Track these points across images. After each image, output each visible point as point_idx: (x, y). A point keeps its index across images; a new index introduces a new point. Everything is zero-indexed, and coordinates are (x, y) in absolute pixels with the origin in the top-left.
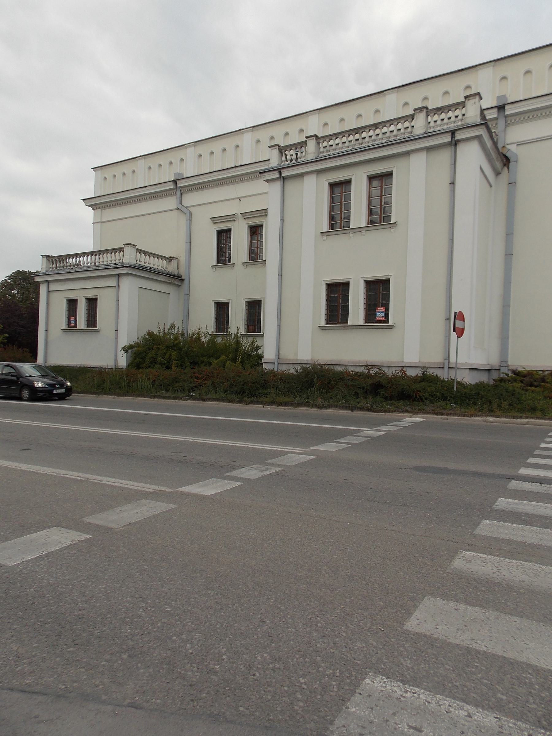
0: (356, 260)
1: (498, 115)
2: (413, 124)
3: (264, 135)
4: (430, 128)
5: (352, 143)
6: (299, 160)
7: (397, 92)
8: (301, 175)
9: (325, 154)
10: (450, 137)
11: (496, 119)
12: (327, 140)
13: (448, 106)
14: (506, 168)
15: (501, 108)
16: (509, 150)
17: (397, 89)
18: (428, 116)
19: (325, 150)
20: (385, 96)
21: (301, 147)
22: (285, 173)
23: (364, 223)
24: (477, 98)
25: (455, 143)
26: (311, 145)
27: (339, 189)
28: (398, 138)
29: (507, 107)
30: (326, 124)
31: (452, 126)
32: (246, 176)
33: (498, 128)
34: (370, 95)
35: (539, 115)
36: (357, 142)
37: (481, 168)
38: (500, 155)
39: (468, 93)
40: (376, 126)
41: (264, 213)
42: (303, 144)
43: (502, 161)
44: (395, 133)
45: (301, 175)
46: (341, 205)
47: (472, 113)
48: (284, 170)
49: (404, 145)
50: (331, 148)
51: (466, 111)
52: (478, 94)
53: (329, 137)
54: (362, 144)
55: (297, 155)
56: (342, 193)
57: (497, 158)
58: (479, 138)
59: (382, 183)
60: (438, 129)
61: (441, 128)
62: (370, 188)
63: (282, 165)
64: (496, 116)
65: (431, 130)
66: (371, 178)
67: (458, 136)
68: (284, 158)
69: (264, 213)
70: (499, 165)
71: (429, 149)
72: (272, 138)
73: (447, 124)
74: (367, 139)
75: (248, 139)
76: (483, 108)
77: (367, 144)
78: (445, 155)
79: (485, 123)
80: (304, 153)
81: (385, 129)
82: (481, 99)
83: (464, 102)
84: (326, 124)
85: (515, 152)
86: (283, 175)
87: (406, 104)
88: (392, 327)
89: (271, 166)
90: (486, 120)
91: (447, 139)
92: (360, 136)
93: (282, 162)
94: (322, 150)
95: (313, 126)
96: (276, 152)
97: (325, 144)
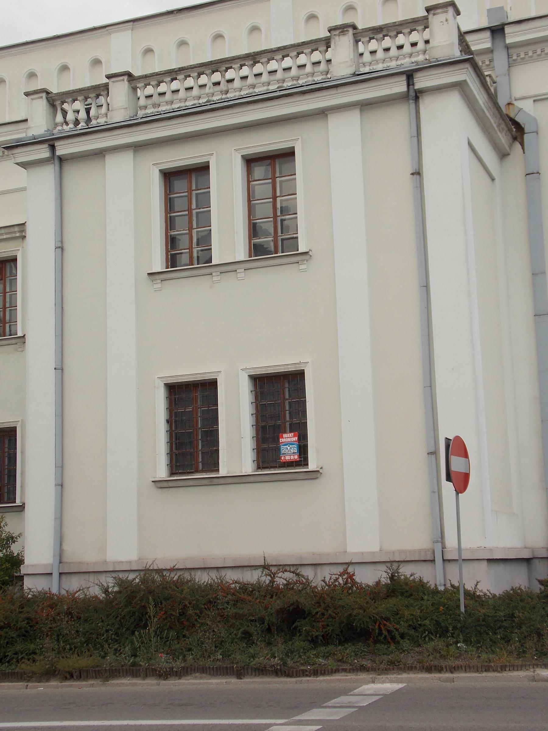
0: (230, 333)
1: (493, 43)
2: (328, 56)
5: (207, 90)
6: (94, 122)
8: (100, 154)
9: (149, 111)
10: (405, 83)
11: (490, 51)
14: (517, 145)
15: (497, 31)
16: (520, 110)
18: (357, 42)
19: (150, 101)
21: (98, 96)
22: (62, 149)
24: (451, 10)
25: (415, 96)
26: (119, 92)
27: (185, 182)
28: (301, 82)
29: (507, 30)
30: (149, 51)
31: (407, 63)
33: (496, 67)
36: (217, 88)
37: (470, 144)
38: (503, 120)
40: (253, 58)
42: (101, 90)
43: (510, 130)
45: (100, 154)
46: (190, 215)
47: (442, 39)
49: (316, 96)
50: (162, 99)
51: (431, 34)
53: (158, 77)
54: (227, 92)
55: (88, 111)
56: (190, 191)
57: (499, 126)
58: (460, 86)
60: (380, 67)
63: (55, 131)
64: (488, 45)
65: (367, 70)
66: (250, 161)
67: (421, 82)
68: (59, 118)
69: (19, 231)
70: (503, 138)
71: (365, 106)
73: (411, 55)
76: (464, 29)
78: (398, 118)
79: (469, 59)
81: (273, 65)
82: (458, 13)
83: (426, 18)
85: (531, 113)
86: (59, 152)
87: (312, 17)
88: (315, 474)
90: (471, 53)
91: (399, 86)
92: (223, 76)
93: (56, 125)
95: (122, 55)
97: (149, 90)
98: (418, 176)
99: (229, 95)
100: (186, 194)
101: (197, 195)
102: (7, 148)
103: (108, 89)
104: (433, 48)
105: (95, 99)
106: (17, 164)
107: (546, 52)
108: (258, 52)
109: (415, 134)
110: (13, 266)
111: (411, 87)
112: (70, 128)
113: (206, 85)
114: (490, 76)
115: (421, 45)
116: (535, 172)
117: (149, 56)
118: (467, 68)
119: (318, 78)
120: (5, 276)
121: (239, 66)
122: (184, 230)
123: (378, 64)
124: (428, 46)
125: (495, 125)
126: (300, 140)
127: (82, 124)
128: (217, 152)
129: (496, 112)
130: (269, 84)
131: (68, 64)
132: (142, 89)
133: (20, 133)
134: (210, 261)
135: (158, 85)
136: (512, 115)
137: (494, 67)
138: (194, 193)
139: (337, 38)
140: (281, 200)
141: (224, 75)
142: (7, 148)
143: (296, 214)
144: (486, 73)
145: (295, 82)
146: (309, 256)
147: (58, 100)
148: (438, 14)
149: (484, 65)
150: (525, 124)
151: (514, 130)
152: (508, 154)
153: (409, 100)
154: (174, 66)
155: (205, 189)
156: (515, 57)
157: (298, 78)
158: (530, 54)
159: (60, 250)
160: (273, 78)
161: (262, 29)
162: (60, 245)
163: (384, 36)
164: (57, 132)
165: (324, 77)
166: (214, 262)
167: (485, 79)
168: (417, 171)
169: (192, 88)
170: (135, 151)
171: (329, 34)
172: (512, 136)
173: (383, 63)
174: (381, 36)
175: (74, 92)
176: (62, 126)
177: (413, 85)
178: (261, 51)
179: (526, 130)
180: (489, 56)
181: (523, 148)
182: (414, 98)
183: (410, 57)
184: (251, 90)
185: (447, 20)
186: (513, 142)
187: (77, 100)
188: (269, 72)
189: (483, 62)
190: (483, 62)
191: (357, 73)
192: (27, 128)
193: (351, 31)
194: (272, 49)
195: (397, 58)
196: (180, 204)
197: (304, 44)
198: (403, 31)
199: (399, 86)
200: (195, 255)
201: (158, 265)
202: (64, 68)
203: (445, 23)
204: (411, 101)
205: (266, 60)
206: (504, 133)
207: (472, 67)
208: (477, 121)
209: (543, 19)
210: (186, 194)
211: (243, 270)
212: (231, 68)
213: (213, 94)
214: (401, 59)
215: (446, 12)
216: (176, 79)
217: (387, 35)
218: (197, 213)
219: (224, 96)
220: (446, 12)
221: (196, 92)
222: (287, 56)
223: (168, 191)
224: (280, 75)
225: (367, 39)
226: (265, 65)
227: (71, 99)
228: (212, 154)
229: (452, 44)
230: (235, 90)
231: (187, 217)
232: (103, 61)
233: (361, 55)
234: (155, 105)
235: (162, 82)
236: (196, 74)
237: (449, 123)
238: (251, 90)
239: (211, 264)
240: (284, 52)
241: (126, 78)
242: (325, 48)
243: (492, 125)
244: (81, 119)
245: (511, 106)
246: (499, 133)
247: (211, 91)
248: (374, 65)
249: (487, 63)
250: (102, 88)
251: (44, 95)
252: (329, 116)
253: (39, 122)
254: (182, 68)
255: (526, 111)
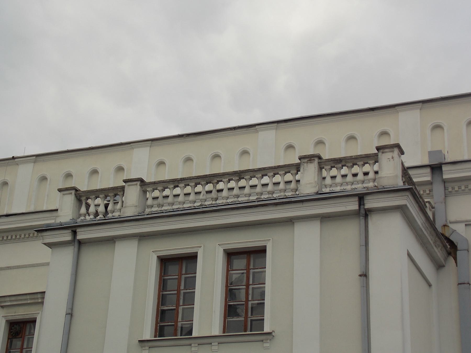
1: (432, 178)
2: (298, 177)
3: (55, 171)
4: (326, 186)
5: (201, 197)
6: (110, 215)
7: (276, 129)
8: (112, 240)
9: (154, 209)
10: (357, 203)
11: (430, 183)
12: (160, 188)
13: (351, 158)
14: (451, 259)
15: (436, 168)
16: (454, 231)
17: (276, 124)
18: (321, 168)
19: (156, 202)
20: (257, 132)
21: (115, 195)
22: (82, 235)
23: (216, 330)
24: (396, 151)
25: (365, 214)
26: (132, 195)
27: (176, 269)
28: (275, 195)
29: (444, 168)
30: (161, 163)
31: (359, 188)
32: (14, 234)
33: (435, 196)
34: (235, 128)
35: (23, 236)
36: (209, 196)
37: (409, 255)
38: (439, 238)
39: (385, 142)
40: (240, 175)
41: (38, 298)
42: (118, 191)
43: (445, 246)
44: (236, 191)
45: (112, 240)
46: (178, 294)
47: (389, 171)
48: (83, 229)
49: (286, 209)
50: (166, 201)
51: (380, 167)
52: (398, 146)
53: (164, 184)
54: (216, 199)
55: (106, 206)
56: (180, 274)
57: (435, 243)
58: (402, 209)
59: (248, 264)
60: (338, 189)
61: (342, 188)
62: (228, 271)
63: (79, 220)
64: (428, 178)
65: (327, 190)
66: (231, 255)
67: (370, 203)
68: (83, 210)
69: (38, 298)
70: (439, 253)
71: (324, 218)
72: (69, 176)
73: (363, 182)
74: (225, 193)
75: (25, 173)
76: (406, 165)
77: (247, 198)
78: (350, 231)
79: (410, 188)
80: (119, 204)
81: (254, 181)
82: (402, 153)
83: (376, 155)
84: (161, 163)
85: (463, 234)
86: (79, 237)
87: (290, 147)
89: (58, 221)
90: (413, 183)
91: (353, 205)
92: (214, 187)
93: (80, 215)
94: (150, 202)
95: (141, 166)
96: (70, 199)
97: (156, 193)
98: (365, 278)
99: (218, 202)
100: (177, 277)
101: (186, 278)
102: (38, 231)
103: (124, 191)
104: (381, 178)
105: (113, 197)
106: (45, 244)
107: (469, 188)
108: (243, 171)
109: (364, 244)
110: (32, 325)
111: (362, 206)
112: (91, 219)
113: (201, 192)
114: (429, 202)
115: (371, 175)
116: (466, 282)
117: (162, 167)
118: (408, 196)
119: (289, 194)
120: (25, 334)
121: (228, 180)
122: (172, 306)
123: (337, 186)
124: (377, 176)
125: (432, 242)
126: (271, 241)
127: (101, 216)
128: (204, 246)
129: (433, 232)
130: (250, 195)
131: (98, 170)
132: (151, 193)
133: (50, 219)
134: (190, 332)
135: (164, 190)
136: (447, 235)
137: (433, 196)
138: (183, 276)
139: (305, 164)
140: (252, 288)
141: (216, 186)
142: (38, 231)
143: (264, 300)
144: (426, 200)
145: (270, 196)
146: (272, 336)
147: (84, 196)
148: (386, 152)
149: (425, 194)
150: (457, 243)
151: (449, 247)
152: (444, 266)
153: (359, 216)
154: (179, 176)
155: (192, 274)
156: (450, 190)
157: (273, 193)
158: (463, 188)
159: (69, 316)
160: (253, 190)
161: (250, 153)
162: (70, 312)
163: (343, 166)
164: (80, 221)
165: (294, 193)
166: (194, 334)
167: (425, 204)
168: (365, 273)
169: (190, 194)
170: (140, 240)
171: (300, 162)
172: (447, 251)
173: (341, 186)
174: (340, 165)
175: (97, 191)
176: (85, 217)
177: (364, 205)
178: (245, 170)
179: (459, 247)
180: (429, 187)
181: (456, 262)
182: (364, 215)
183: (363, 183)
184: (236, 199)
185: (393, 158)
186: (448, 256)
187: (99, 197)
188: (251, 186)
189: (424, 191)
190: (424, 191)
191: (319, 192)
192: (57, 217)
193: (317, 160)
194: (254, 169)
195: (352, 184)
196: (172, 284)
197: (279, 167)
198: (358, 163)
199: (353, 205)
200: (250, 306)
201: (148, 334)
202: (95, 172)
203: (391, 160)
204: (362, 218)
205: (249, 177)
206: (439, 249)
207: (420, 193)
208: (416, 237)
209: (459, 164)
210: (177, 277)
211: (217, 344)
212: (221, 181)
213: (206, 200)
214: (356, 184)
215: (393, 152)
216: (178, 186)
217: (345, 166)
218: (184, 293)
219: (214, 202)
220: (393, 152)
221: (192, 197)
222: (266, 175)
223: (163, 274)
224: (259, 189)
225: (329, 167)
226: (248, 181)
227: (94, 196)
228: (200, 247)
229: (396, 176)
230: (223, 198)
231: (176, 296)
232: (125, 168)
233: (324, 178)
234: (159, 205)
235: (167, 188)
236: (193, 184)
237: (392, 239)
238: (236, 199)
239: (191, 337)
240: (263, 173)
241: (139, 183)
242: (296, 172)
243: (429, 242)
244: (100, 212)
245: (446, 227)
246: (435, 248)
247: (204, 197)
248: (334, 187)
249: (428, 192)
250: (119, 190)
251: (73, 192)
252: (295, 224)
253: (67, 211)
254: (183, 178)
255: (460, 232)
